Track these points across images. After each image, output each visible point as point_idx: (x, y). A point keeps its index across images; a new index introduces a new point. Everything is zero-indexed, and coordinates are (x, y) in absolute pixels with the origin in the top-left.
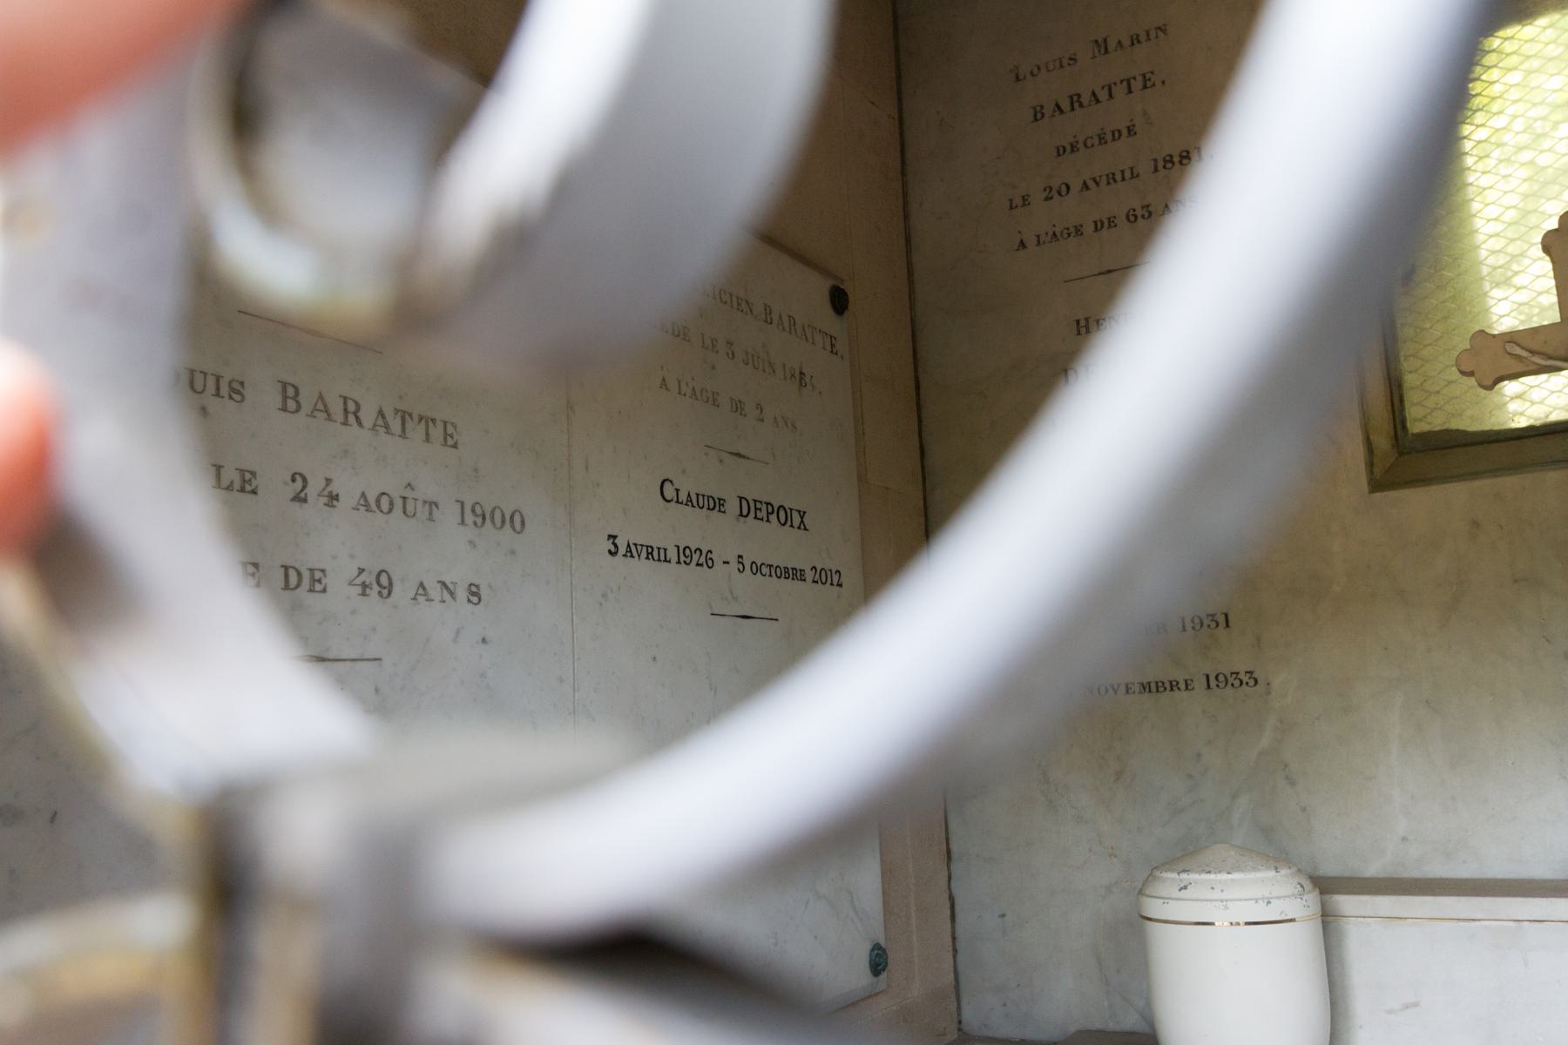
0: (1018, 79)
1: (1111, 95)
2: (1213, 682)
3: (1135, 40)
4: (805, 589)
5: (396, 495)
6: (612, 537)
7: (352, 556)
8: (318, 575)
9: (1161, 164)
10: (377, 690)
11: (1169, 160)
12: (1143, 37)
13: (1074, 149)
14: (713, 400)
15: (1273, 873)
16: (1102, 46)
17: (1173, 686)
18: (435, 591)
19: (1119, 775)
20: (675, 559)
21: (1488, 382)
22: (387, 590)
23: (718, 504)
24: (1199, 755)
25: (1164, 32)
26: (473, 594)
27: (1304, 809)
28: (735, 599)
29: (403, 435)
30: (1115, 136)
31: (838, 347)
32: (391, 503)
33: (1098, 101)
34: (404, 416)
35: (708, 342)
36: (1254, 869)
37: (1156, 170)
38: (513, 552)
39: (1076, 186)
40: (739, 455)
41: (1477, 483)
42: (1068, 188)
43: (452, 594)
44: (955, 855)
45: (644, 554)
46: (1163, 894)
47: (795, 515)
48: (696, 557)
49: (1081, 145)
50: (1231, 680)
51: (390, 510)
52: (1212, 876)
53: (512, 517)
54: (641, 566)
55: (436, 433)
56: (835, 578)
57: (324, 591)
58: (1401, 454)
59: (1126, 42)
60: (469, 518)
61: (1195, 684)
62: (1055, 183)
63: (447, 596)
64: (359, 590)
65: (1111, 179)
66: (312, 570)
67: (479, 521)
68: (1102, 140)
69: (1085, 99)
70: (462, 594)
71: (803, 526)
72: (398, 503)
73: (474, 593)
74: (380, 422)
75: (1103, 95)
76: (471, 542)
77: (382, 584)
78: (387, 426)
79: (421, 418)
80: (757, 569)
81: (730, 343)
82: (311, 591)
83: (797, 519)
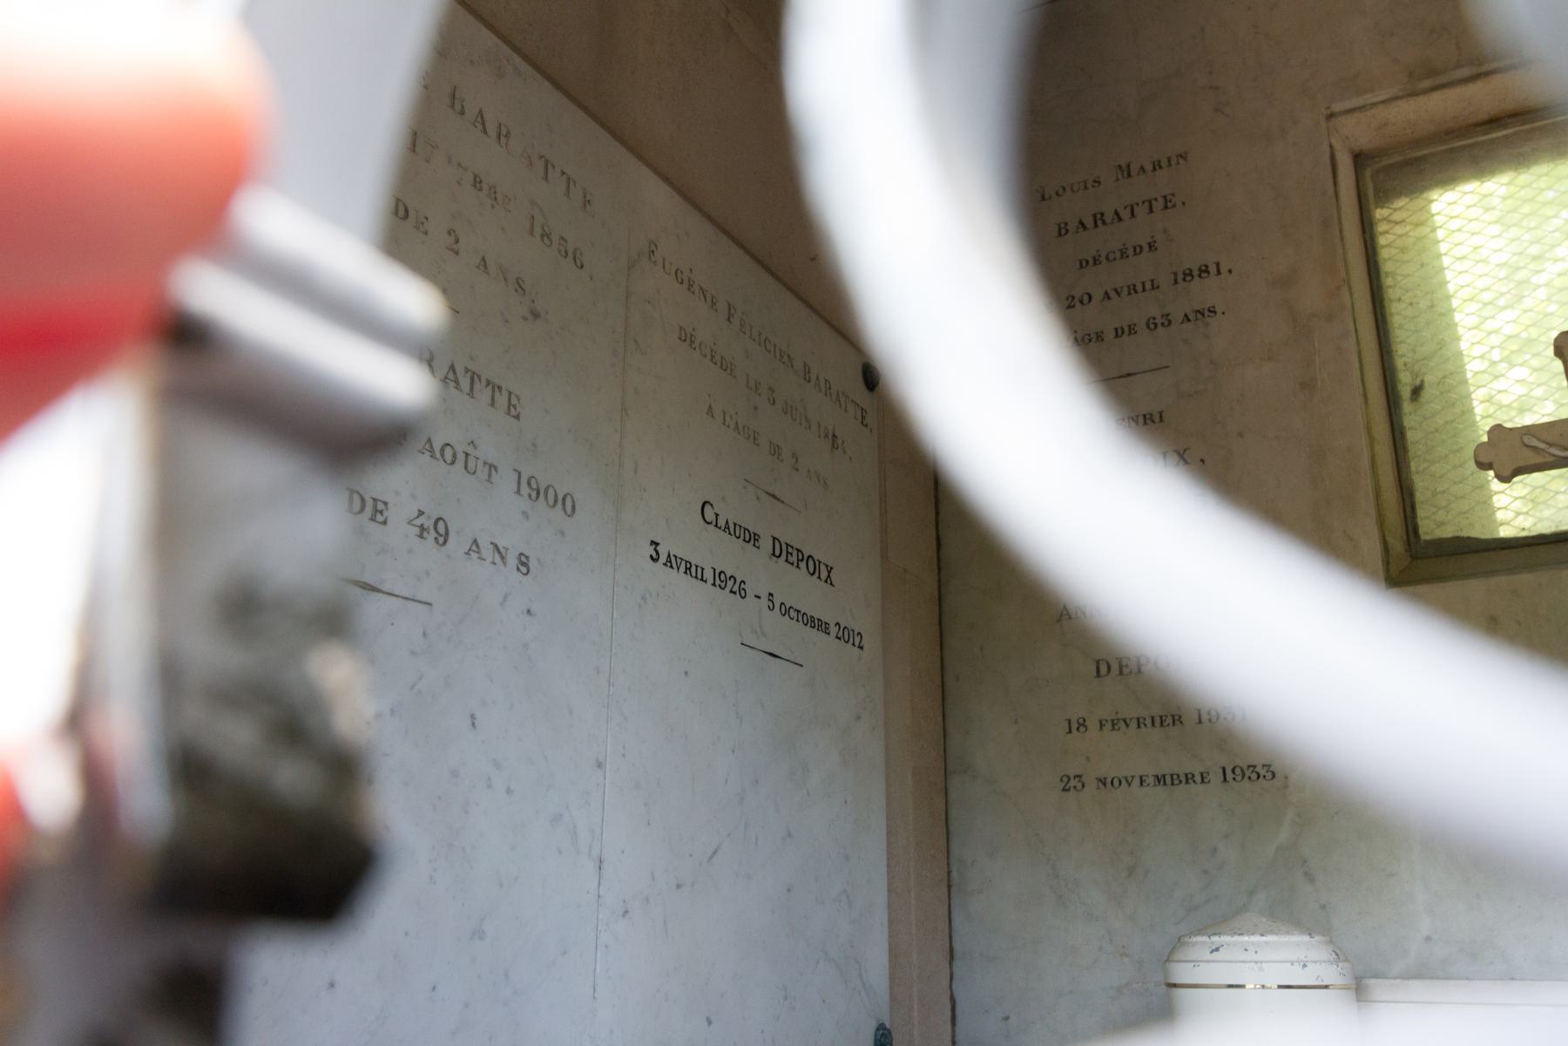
0: (1043, 198)
1: (1133, 215)
2: (1230, 776)
3: (1157, 166)
4: (828, 642)
5: (460, 449)
6: (654, 543)
7: (414, 496)
8: (380, 506)
9: (1180, 277)
10: (425, 634)
11: (1188, 274)
12: (1164, 163)
13: (1096, 261)
14: (754, 438)
15: (1306, 938)
16: (1126, 171)
17: (1189, 778)
18: (487, 551)
19: (1131, 871)
20: (711, 581)
21: (1507, 473)
22: (443, 538)
23: (753, 539)
24: (1215, 850)
25: (1185, 159)
26: (523, 564)
27: (1323, 907)
28: (764, 634)
29: (471, 393)
30: (1138, 250)
31: (867, 421)
32: (454, 456)
33: (1120, 219)
34: (474, 377)
35: (752, 384)
36: (1287, 933)
37: (1176, 282)
38: (562, 533)
39: (1098, 295)
40: (774, 496)
41: (1493, 581)
42: (1090, 298)
43: (503, 558)
44: (957, 953)
45: (682, 569)
46: (1194, 957)
47: (823, 568)
48: (730, 583)
49: (1103, 259)
50: (1248, 773)
51: (453, 463)
52: (1246, 938)
53: (564, 499)
54: (677, 578)
55: (502, 400)
56: (857, 639)
57: (385, 523)
58: (1414, 558)
59: (1149, 167)
60: (525, 490)
61: (1212, 777)
62: (1078, 293)
63: (498, 559)
64: (417, 531)
65: (1133, 289)
66: (375, 500)
67: (534, 495)
68: (1124, 254)
69: (1109, 217)
70: (512, 561)
71: (828, 580)
72: (461, 457)
73: (523, 563)
74: (451, 376)
75: (1125, 214)
76: (524, 513)
77: (437, 530)
78: (456, 382)
79: (488, 383)
80: (786, 611)
81: (771, 390)
82: (373, 519)
83: (824, 574)
